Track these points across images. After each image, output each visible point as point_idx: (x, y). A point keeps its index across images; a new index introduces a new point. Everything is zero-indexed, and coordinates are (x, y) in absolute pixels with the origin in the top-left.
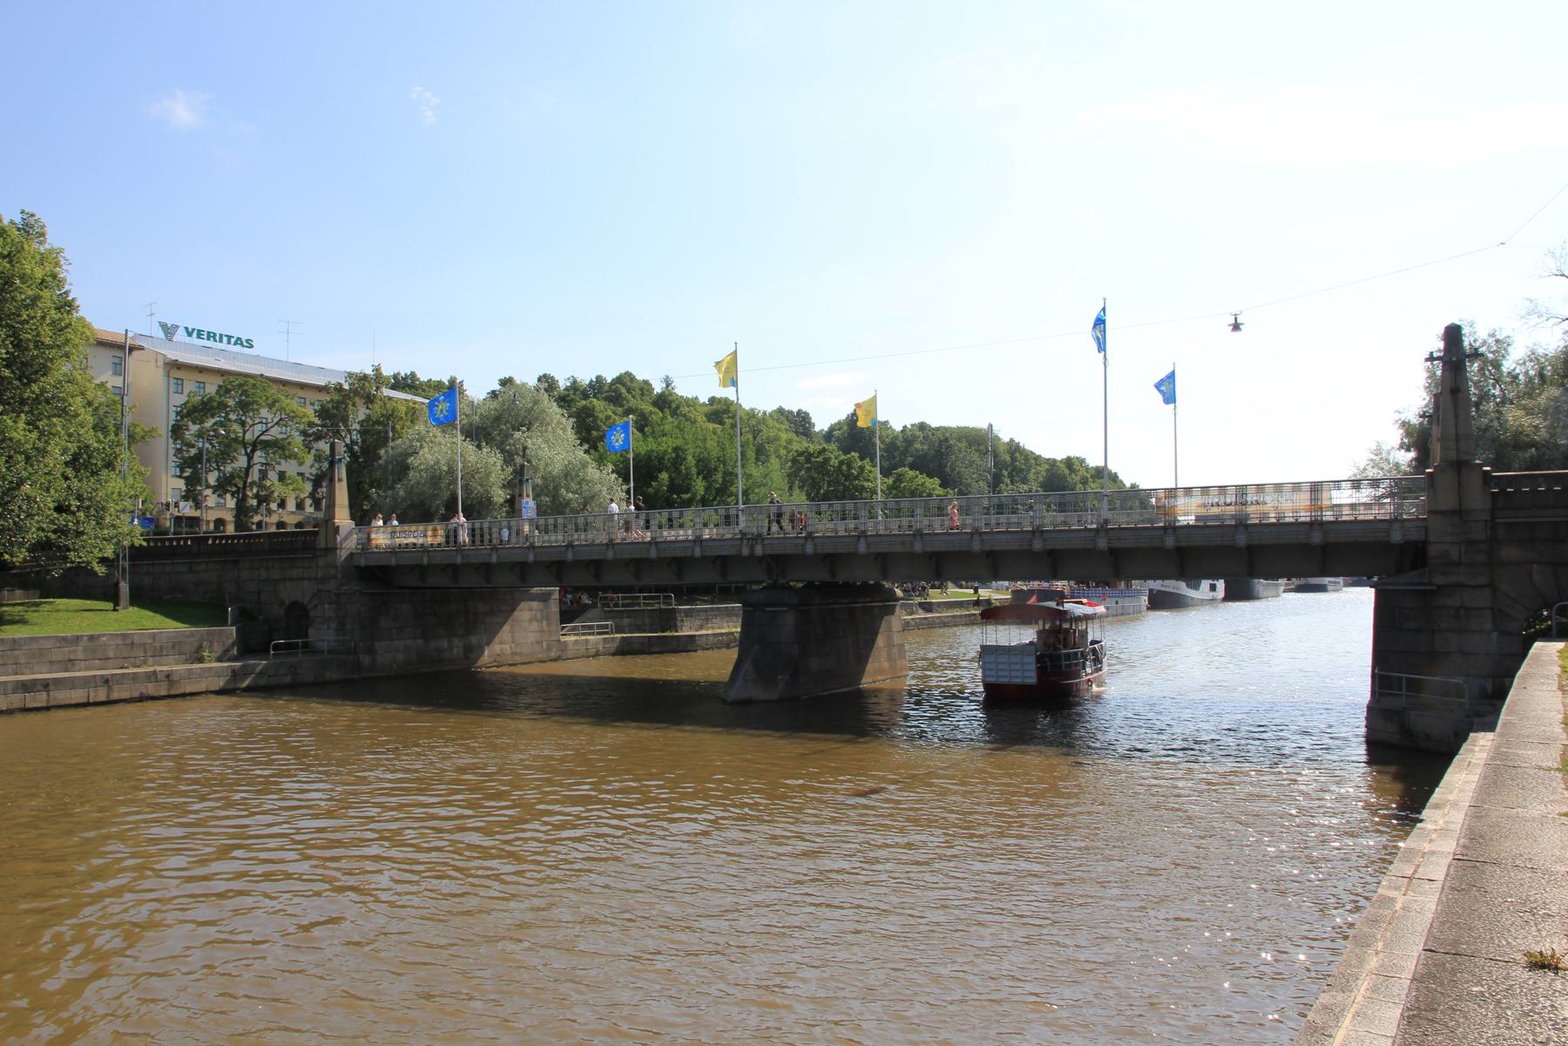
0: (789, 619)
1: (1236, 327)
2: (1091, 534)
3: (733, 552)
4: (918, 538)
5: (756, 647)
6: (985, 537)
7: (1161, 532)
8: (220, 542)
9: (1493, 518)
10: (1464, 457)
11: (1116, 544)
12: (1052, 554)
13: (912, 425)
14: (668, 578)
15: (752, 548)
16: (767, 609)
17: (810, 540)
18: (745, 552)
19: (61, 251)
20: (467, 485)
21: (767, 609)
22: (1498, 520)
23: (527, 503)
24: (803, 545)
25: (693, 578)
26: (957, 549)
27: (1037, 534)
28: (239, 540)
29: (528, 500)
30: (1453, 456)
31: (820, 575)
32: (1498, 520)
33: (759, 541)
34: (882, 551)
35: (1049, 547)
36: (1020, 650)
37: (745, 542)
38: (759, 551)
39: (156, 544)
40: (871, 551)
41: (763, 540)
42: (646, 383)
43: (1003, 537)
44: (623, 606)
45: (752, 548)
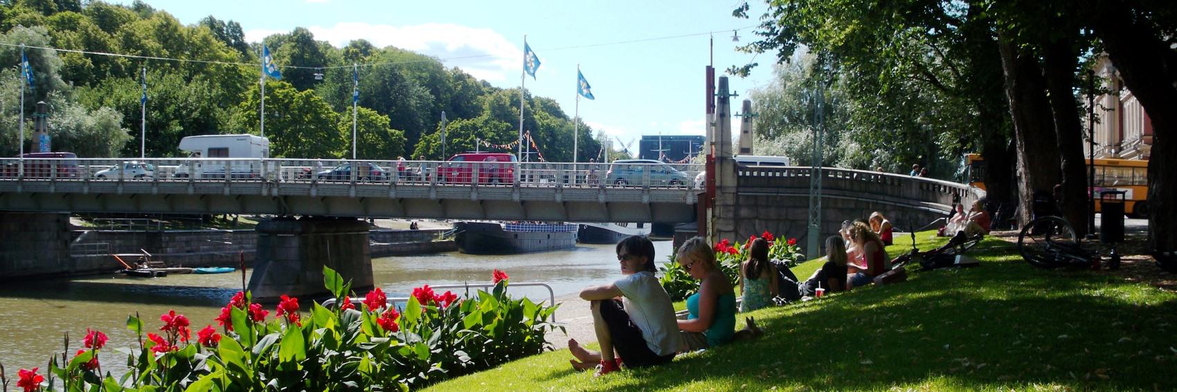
0: (295, 242)
3: (254, 192)
4: (393, 188)
5: (271, 262)
6: (439, 190)
8: (804, 174)
9: (738, 192)
10: (725, 155)
11: (524, 198)
12: (239, 197)
13: (536, 97)
14: (130, 208)
15: (270, 190)
16: (279, 235)
17: (314, 186)
18: (265, 192)
21: (279, 235)
22: (739, 193)
23: (44, 137)
24: (309, 190)
25: (114, 207)
26: (420, 197)
27: (558, 191)
28: (797, 174)
29: (44, 134)
30: (720, 155)
31: (318, 210)
32: (739, 193)
33: (276, 186)
34: (366, 196)
35: (481, 199)
37: (264, 185)
38: (275, 192)
39: (774, 174)
41: (649, 191)
44: (134, 227)
45: (270, 190)
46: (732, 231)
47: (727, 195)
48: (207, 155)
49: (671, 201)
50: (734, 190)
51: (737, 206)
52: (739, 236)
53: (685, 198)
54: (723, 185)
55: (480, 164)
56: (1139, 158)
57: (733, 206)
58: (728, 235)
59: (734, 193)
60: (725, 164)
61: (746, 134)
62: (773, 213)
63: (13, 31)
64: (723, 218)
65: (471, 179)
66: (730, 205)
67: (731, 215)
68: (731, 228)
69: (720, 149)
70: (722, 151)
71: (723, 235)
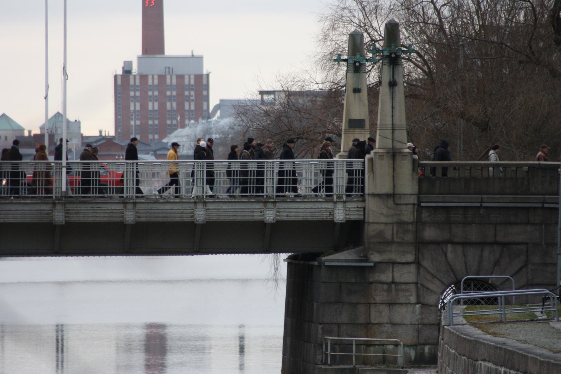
9: (419, 201)
22: (423, 204)
46: (413, 263)
47: (404, 207)
48: (125, 159)
49: (309, 218)
50: (413, 200)
51: (419, 223)
52: (422, 270)
53: (332, 213)
54: (395, 192)
55: (328, 162)
56: (411, 295)
57: (412, 223)
58: (406, 268)
59: (414, 204)
60: (398, 158)
61: (357, 94)
62: (474, 233)
63: (288, 88)
64: (398, 243)
65: (332, 179)
66: (408, 223)
67: (409, 237)
68: (410, 258)
69: (390, 136)
70: (393, 139)
71: (397, 269)
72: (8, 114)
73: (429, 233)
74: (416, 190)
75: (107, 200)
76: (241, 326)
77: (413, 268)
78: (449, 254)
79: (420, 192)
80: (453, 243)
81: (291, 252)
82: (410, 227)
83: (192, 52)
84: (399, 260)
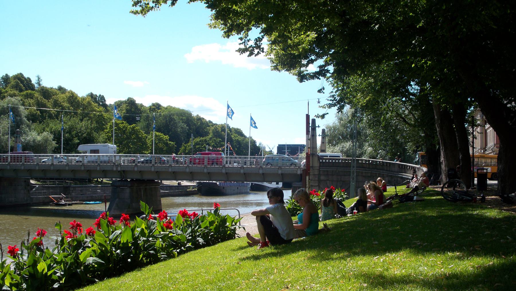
0: (128, 191)
1: (89, 26)
2: (221, 168)
5: (117, 199)
7: (240, 169)
9: (320, 169)
11: (227, 171)
13: (232, 128)
15: (117, 168)
17: (136, 166)
18: (115, 169)
19: (276, 68)
20: (103, 142)
23: (19, 145)
24: (134, 168)
29: (19, 144)
31: (138, 177)
36: (495, 184)
37: (115, 166)
38: (119, 169)
40: (155, 170)
42: (29, 78)
43: (196, 168)
45: (117, 168)
50: (318, 168)
51: (319, 175)
53: (297, 171)
66: (316, 175)
67: (317, 179)
68: (317, 184)
72: (63, 86)
73: (322, 178)
74: (319, 165)
75: (27, 153)
76: (189, 2)
77: (317, 187)
78: (328, 184)
79: (320, 166)
80: (329, 181)
81: (498, 256)
82: (317, 176)
83: (237, 51)
84: (313, 185)
